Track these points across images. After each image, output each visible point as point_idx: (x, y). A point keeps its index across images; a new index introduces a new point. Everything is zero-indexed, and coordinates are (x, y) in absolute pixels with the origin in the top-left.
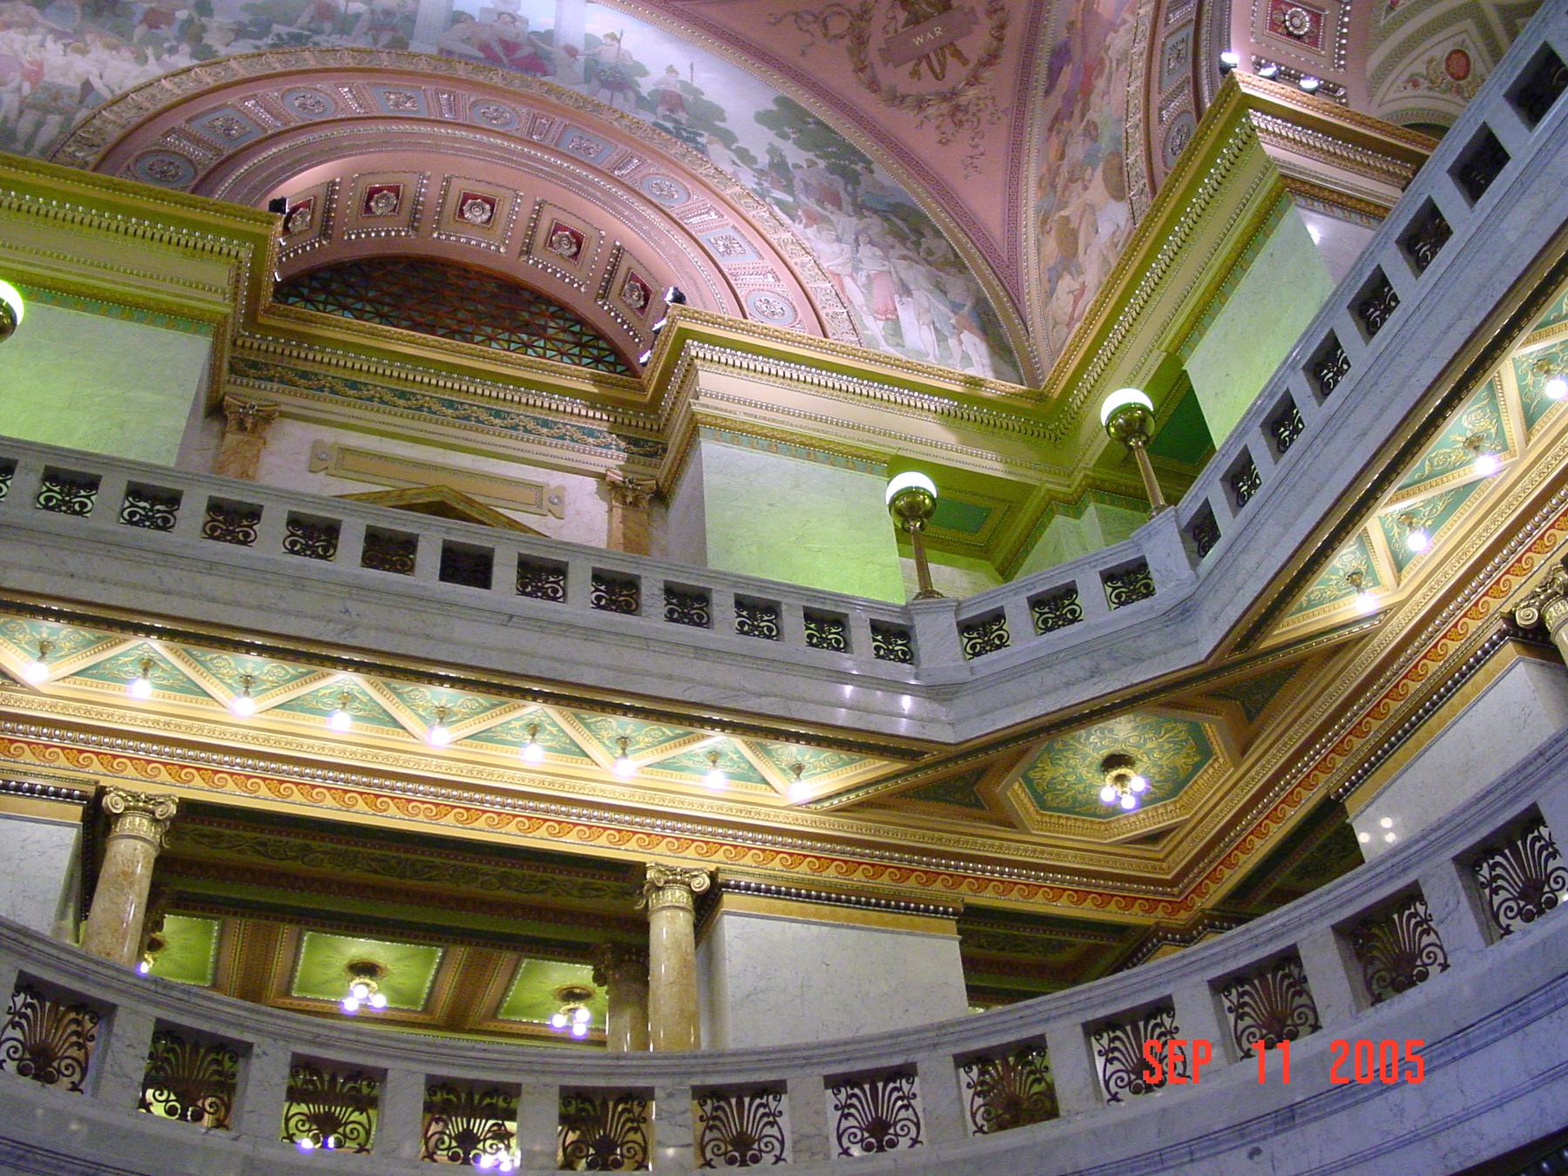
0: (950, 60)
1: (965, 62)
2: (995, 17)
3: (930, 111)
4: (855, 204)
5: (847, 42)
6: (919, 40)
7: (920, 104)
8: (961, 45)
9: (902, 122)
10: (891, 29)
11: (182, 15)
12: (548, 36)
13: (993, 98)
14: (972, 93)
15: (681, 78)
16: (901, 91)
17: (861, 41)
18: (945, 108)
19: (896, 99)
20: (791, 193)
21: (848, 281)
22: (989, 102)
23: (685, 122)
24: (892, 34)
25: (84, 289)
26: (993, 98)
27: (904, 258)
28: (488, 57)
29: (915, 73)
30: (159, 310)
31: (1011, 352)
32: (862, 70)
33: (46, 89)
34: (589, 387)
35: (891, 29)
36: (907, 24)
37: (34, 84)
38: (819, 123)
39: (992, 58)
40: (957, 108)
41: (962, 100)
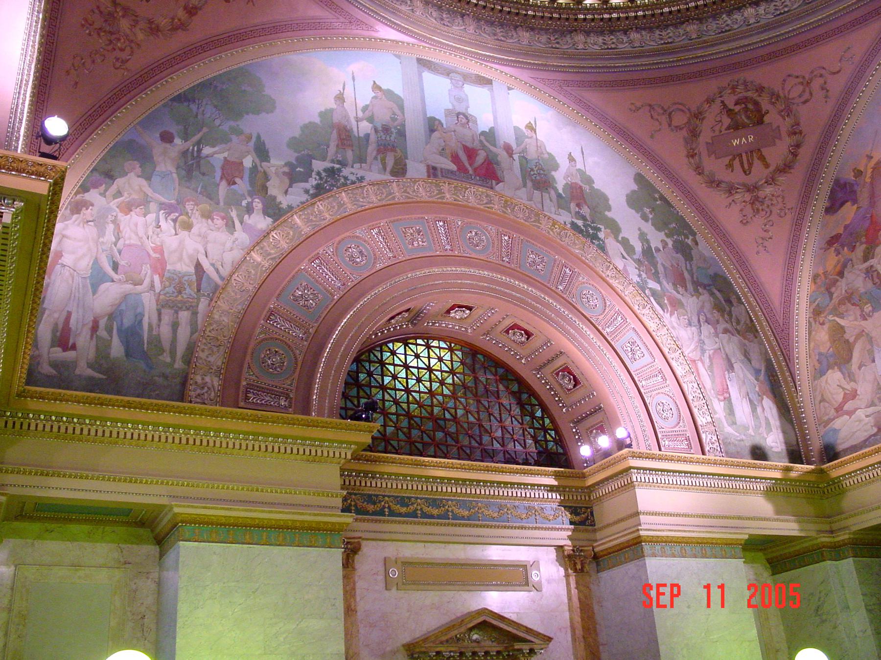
0: (757, 162)
1: (767, 166)
2: (795, 138)
3: (737, 196)
4: (693, 282)
5: (684, 133)
6: (736, 142)
7: (731, 190)
8: (765, 151)
9: (715, 200)
10: (717, 128)
11: (248, 162)
12: (490, 135)
13: (783, 198)
14: (768, 190)
15: (578, 167)
16: (718, 177)
17: (694, 134)
18: (748, 197)
19: (714, 183)
20: (659, 282)
21: (700, 364)
22: (780, 200)
23: (586, 212)
24: (717, 133)
25: (249, 521)
26: (783, 198)
27: (726, 331)
28: (459, 169)
29: (730, 166)
30: (303, 528)
31: (789, 411)
32: (692, 156)
33: (170, 279)
34: (552, 481)
35: (717, 128)
36: (728, 128)
37: (162, 276)
38: (662, 198)
39: (785, 168)
40: (757, 198)
41: (761, 194)
